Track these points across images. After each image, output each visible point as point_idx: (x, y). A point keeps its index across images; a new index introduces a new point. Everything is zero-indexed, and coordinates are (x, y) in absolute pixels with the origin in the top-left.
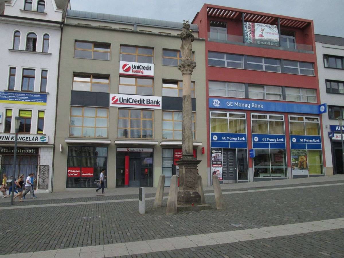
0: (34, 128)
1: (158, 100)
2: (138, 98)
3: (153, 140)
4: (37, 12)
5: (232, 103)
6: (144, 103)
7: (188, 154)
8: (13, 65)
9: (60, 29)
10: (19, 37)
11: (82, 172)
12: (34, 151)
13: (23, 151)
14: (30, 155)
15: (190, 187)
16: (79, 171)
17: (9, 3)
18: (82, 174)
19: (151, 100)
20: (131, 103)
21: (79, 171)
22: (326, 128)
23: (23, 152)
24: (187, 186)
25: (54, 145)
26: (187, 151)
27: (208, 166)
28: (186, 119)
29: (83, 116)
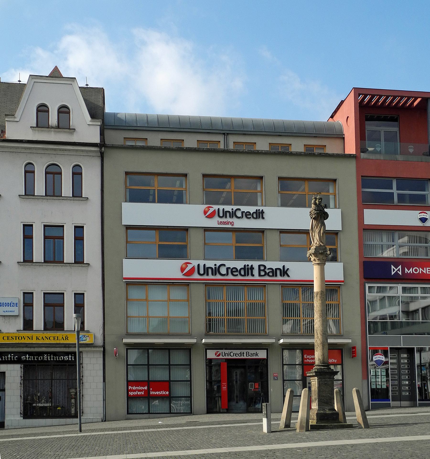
0: (70, 319)
1: (284, 267)
2: (239, 264)
3: (266, 336)
4: (58, 127)
5: (428, 269)
6: (253, 275)
8: (28, 221)
9: (99, 154)
10: (33, 172)
11: (151, 389)
12: (73, 357)
13: (56, 358)
14: (67, 364)
16: (146, 388)
17: (13, 116)
18: (151, 393)
19: (267, 267)
20: (224, 275)
21: (146, 388)
23: (55, 360)
25: (104, 347)
27: (363, 378)
29: (146, 300)
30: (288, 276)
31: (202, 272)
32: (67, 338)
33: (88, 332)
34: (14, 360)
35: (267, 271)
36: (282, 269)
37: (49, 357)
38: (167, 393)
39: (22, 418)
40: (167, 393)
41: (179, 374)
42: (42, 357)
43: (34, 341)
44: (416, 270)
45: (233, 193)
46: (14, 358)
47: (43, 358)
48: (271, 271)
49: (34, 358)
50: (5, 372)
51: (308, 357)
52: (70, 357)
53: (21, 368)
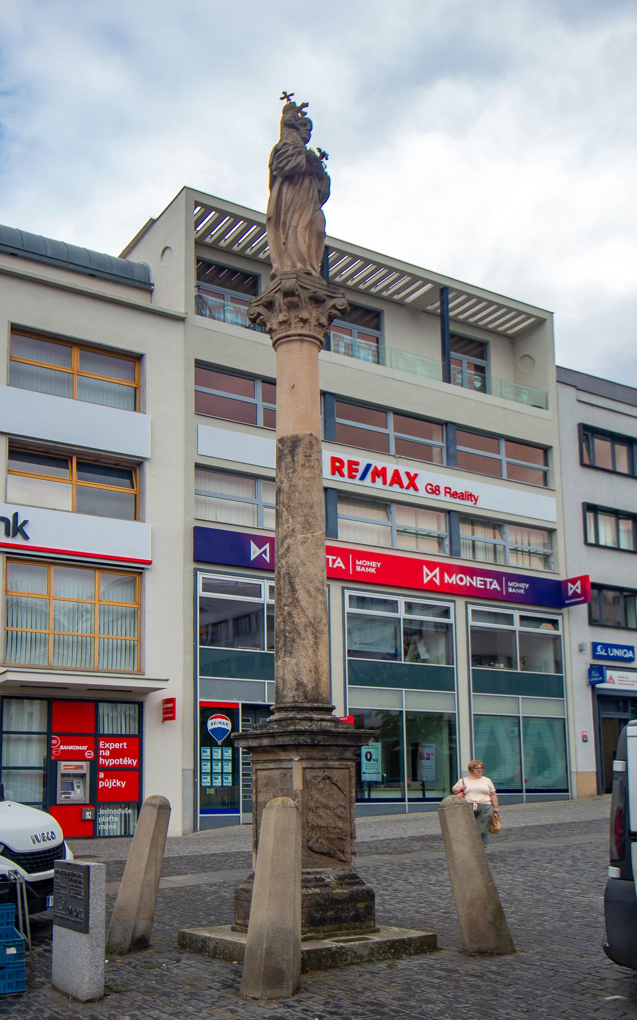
1: (16, 516)
7: (312, 701)
15: (328, 855)
22: (580, 651)
24: (310, 849)
26: (310, 686)
28: (303, 543)
30: (26, 537)
44: (461, 580)
51: (107, 745)
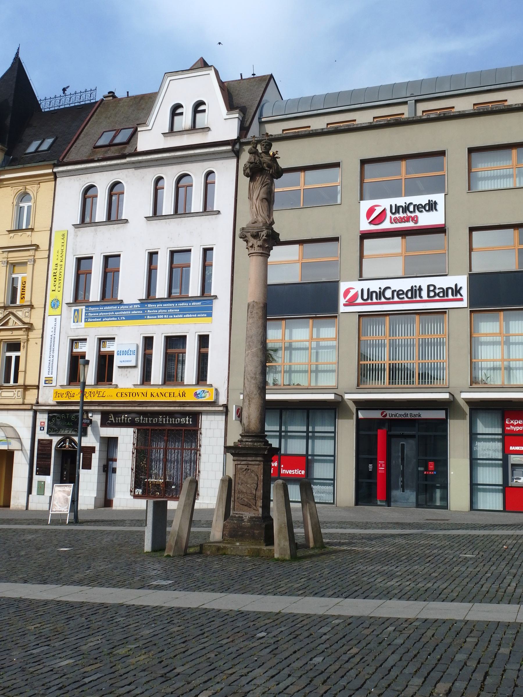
1: (456, 285)
2: (405, 285)
11: (282, 466)
12: (191, 419)
14: (183, 428)
18: (283, 471)
19: (437, 287)
23: (171, 422)
31: (365, 297)
32: (184, 395)
33: (211, 386)
34: (127, 423)
35: (437, 291)
36: (454, 288)
37: (164, 419)
38: (303, 472)
39: (132, 497)
40: (303, 472)
41: (322, 447)
42: (157, 419)
43: (149, 399)
45: (403, 180)
46: (127, 420)
47: (158, 420)
48: (442, 290)
49: (148, 420)
50: (117, 438)
52: (187, 419)
53: (134, 432)
